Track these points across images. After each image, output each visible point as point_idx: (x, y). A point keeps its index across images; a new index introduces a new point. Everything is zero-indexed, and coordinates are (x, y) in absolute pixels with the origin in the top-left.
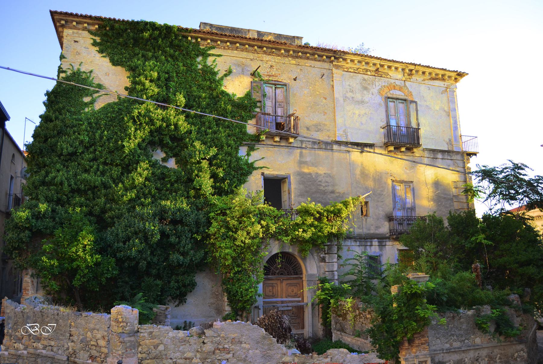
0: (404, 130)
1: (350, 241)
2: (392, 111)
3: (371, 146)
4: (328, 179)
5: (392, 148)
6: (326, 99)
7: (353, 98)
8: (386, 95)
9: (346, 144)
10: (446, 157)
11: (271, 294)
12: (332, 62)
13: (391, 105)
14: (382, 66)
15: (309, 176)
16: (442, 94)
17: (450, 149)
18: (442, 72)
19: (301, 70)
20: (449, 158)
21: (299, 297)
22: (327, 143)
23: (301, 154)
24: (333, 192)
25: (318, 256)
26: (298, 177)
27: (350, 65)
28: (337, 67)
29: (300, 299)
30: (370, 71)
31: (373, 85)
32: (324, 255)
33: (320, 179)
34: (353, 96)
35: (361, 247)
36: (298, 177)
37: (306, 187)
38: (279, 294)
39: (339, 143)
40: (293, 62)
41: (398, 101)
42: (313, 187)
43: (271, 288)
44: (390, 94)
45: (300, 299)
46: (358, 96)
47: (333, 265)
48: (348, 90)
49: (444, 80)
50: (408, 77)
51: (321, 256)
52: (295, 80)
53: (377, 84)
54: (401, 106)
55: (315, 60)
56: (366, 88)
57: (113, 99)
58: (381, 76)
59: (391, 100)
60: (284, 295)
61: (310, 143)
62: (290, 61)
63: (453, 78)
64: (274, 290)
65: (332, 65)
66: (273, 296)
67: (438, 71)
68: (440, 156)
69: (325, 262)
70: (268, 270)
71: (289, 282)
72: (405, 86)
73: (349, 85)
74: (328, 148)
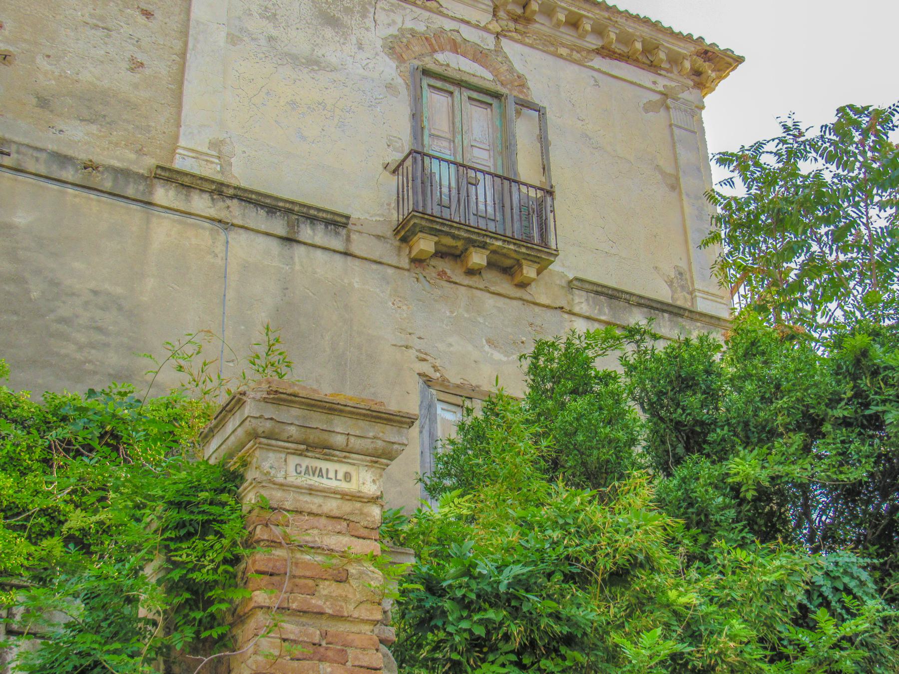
0: (484, 195)
3: (337, 222)
5: (425, 244)
6: (147, 14)
7: (270, 39)
8: (417, 63)
9: (218, 190)
15: (11, 288)
16: (647, 111)
18: (646, 32)
22: (123, 174)
31: (364, 16)
33: (64, 311)
34: (274, 33)
39: (186, 183)
41: (466, 93)
44: (436, 62)
46: (299, 40)
49: (653, 67)
50: (512, 25)
53: (382, 17)
54: (479, 121)
56: (332, 22)
57: (805, 597)
61: (43, 156)
63: (687, 65)
67: (630, 28)
72: (498, 50)
74: (130, 191)
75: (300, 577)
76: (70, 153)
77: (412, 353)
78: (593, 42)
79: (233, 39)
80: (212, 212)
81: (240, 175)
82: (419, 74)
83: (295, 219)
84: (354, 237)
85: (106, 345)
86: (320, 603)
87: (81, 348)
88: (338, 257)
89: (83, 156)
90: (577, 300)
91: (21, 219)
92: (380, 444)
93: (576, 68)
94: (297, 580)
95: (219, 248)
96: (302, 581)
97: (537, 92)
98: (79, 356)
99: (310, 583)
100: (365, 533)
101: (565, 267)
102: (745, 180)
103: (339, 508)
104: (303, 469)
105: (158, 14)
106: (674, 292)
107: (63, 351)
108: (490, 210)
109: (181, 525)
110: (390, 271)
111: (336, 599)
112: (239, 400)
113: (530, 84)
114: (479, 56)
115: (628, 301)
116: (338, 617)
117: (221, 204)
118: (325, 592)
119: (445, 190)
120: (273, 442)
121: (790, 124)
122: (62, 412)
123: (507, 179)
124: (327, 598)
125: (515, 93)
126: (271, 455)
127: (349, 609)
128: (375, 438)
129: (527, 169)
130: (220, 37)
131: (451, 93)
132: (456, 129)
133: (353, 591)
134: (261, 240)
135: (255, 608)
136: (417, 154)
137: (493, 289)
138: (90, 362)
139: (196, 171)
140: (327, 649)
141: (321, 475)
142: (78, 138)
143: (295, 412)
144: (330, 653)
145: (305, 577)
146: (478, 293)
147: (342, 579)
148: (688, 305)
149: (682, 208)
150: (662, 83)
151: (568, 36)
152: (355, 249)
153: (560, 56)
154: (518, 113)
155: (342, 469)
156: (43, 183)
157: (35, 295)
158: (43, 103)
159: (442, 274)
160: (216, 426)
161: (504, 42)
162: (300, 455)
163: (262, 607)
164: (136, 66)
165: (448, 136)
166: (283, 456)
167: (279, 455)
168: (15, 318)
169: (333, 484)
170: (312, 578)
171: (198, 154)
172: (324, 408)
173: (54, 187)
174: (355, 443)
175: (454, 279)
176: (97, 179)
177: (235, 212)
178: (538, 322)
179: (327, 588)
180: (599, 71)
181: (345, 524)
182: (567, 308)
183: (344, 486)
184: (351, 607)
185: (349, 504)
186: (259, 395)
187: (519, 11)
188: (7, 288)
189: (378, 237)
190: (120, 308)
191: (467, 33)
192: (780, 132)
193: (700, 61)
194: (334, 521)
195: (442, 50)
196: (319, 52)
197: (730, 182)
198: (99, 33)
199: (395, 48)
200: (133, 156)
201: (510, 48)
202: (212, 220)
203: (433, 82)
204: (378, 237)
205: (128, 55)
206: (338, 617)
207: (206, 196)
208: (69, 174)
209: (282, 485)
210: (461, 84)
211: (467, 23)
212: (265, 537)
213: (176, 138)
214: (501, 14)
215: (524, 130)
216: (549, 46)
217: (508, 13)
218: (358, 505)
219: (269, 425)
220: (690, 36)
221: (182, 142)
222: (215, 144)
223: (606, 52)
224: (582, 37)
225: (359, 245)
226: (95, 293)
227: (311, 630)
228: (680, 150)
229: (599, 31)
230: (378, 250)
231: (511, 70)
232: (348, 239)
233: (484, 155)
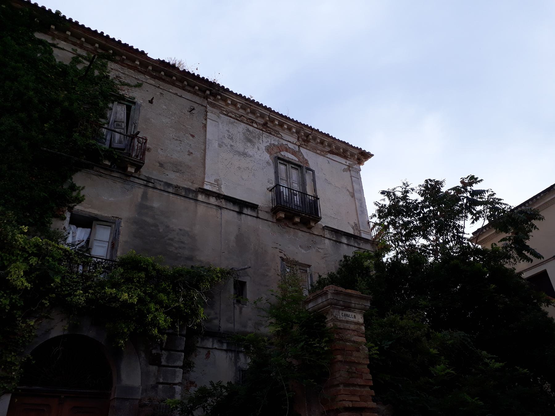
0: (297, 199)
1: (211, 340)
2: (283, 174)
3: (254, 207)
6: (193, 136)
7: (231, 146)
8: (276, 155)
9: (219, 196)
10: (352, 243)
12: (206, 98)
13: (282, 167)
14: (272, 120)
15: (153, 228)
17: (357, 234)
19: (161, 94)
20: (356, 245)
22: (188, 190)
23: (145, 196)
24: (190, 258)
27: (231, 108)
28: (213, 106)
30: (256, 123)
31: (259, 139)
32: (159, 352)
34: (232, 144)
35: (230, 354)
39: (208, 193)
40: (152, 81)
41: (291, 165)
46: (240, 147)
47: (175, 372)
48: (226, 135)
49: (345, 157)
50: (303, 143)
51: (154, 352)
52: (151, 102)
53: (264, 139)
54: (295, 174)
55: (183, 88)
56: (250, 141)
58: (270, 133)
59: (282, 162)
61: (162, 183)
62: (147, 79)
63: (356, 157)
65: (206, 101)
67: (339, 144)
68: (344, 240)
69: (159, 365)
72: (299, 151)
73: (228, 131)
74: (190, 196)
76: (171, 182)
77: (278, 250)
78: (328, 149)
79: (220, 146)
80: (216, 203)
81: (225, 191)
82: (277, 158)
83: (241, 205)
84: (259, 212)
87: (176, 248)
88: (255, 218)
89: (175, 183)
91: (156, 205)
93: (322, 157)
95: (219, 215)
97: (312, 166)
100: (361, 335)
101: (324, 222)
102: (389, 199)
105: (196, 136)
106: (354, 231)
107: (171, 250)
108: (298, 203)
110: (270, 223)
113: (309, 162)
114: (294, 153)
116: (359, 363)
117: (219, 201)
119: (285, 196)
121: (405, 182)
123: (304, 194)
125: (305, 165)
129: (309, 191)
130: (216, 145)
131: (286, 165)
132: (288, 177)
134: (232, 212)
136: (277, 185)
138: (180, 253)
139: (211, 189)
142: (173, 178)
143: (342, 297)
146: (296, 230)
147: (358, 350)
148: (359, 235)
149: (355, 203)
150: (348, 162)
151: (320, 147)
152: (260, 216)
153: (318, 153)
154: (306, 172)
155: (353, 314)
156: (162, 193)
157: (161, 230)
158: (161, 165)
159: (286, 224)
161: (301, 149)
164: (190, 154)
165: (285, 179)
169: (352, 319)
171: (211, 184)
173: (166, 194)
176: (180, 191)
177: (223, 203)
178: (314, 240)
179: (355, 354)
180: (329, 158)
187: (305, 138)
189: (266, 212)
191: (290, 145)
192: (402, 185)
193: (360, 155)
195: (283, 151)
196: (246, 151)
197: (384, 200)
198: (178, 142)
199: (269, 149)
200: (190, 184)
201: (303, 150)
202: (216, 206)
203: (281, 161)
204: (266, 212)
205: (187, 150)
207: (214, 198)
208: (170, 190)
210: (289, 162)
211: (290, 142)
213: (204, 178)
214: (300, 139)
215: (308, 178)
216: (314, 150)
217: (302, 139)
219: (335, 301)
220: (357, 147)
221: (206, 180)
222: (216, 181)
223: (331, 152)
224: (324, 147)
225: (261, 215)
226: (180, 230)
228: (354, 184)
229: (330, 145)
230: (266, 216)
231: (303, 158)
232: (258, 213)
233: (296, 185)
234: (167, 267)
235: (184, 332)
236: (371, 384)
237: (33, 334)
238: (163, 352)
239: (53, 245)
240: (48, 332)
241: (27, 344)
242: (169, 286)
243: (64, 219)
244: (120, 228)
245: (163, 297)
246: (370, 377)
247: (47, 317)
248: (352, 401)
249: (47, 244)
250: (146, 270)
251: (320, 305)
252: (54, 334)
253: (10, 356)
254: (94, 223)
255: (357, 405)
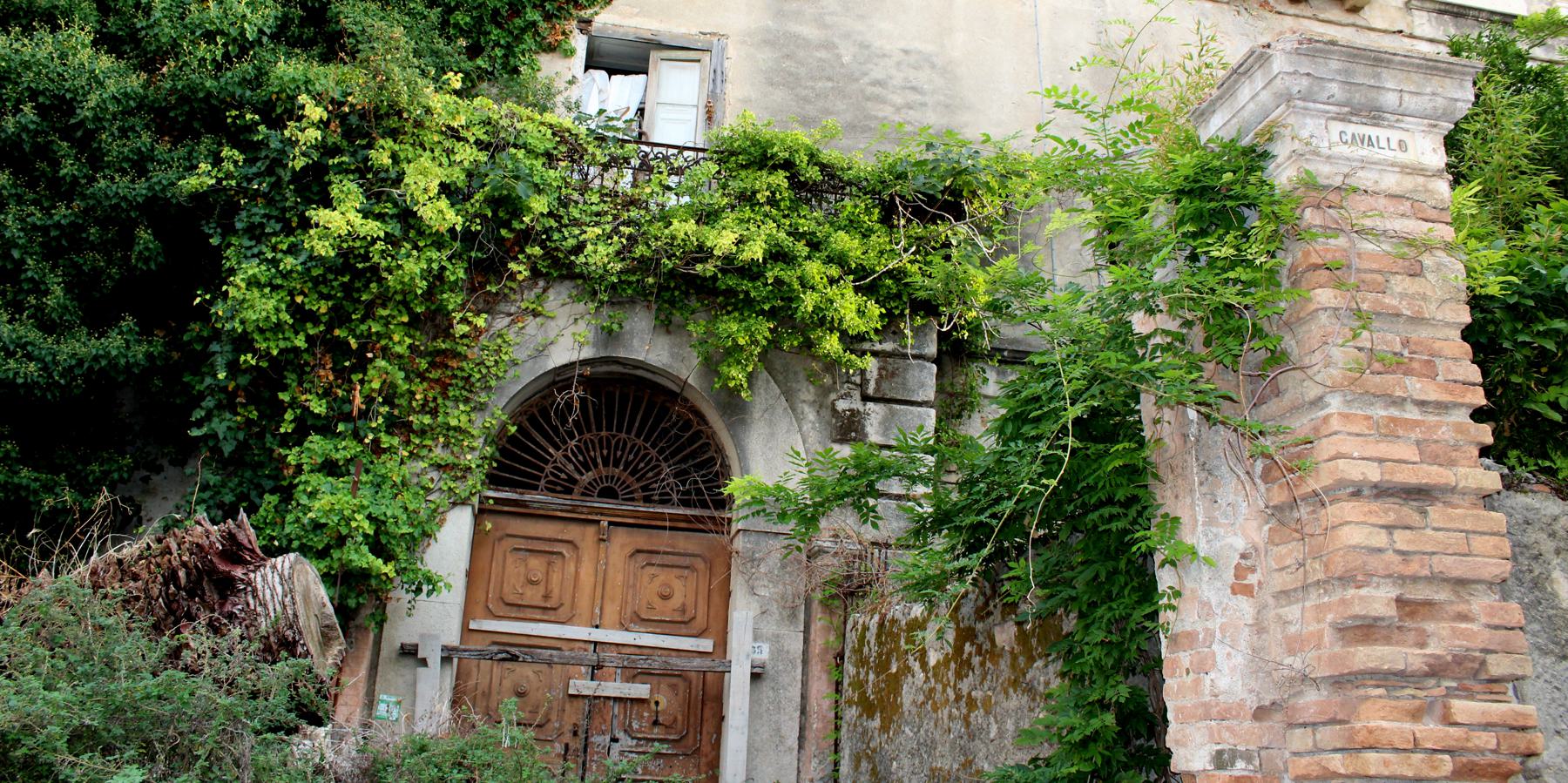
4: (923, 77)
11: (533, 596)
15: (823, 54)
21: (699, 635)
25: (819, 405)
26: (765, 56)
29: (706, 645)
32: (857, 404)
33: (878, 74)
36: (765, 56)
37: (806, 100)
38: (584, 601)
42: (841, 106)
43: (536, 563)
45: (706, 645)
51: (842, 405)
60: (611, 611)
64: (555, 578)
66: (547, 611)
70: (516, 463)
71: (642, 539)
75: (1365, 271)
85: (924, 105)
86: (1395, 302)
87: (898, 110)
90: (1417, 21)
92: (1440, 101)
94: (1363, 276)
96: (1368, 277)
98: (897, 118)
99: (1379, 278)
100: (1433, 214)
103: (1398, 184)
104: (1349, 137)
107: (881, 114)
109: (1198, 217)
111: (1412, 297)
112: (1262, 54)
115: (1476, 18)
116: (1417, 320)
118: (1399, 289)
120: (1311, 105)
122: (900, 169)
124: (1403, 296)
126: (1308, 121)
127: (1430, 310)
128: (1434, 94)
133: (1431, 285)
135: (1317, 310)
137: (1322, 16)
140: (1411, 359)
141: (1370, 143)
144: (1415, 365)
145: (1372, 271)
155: (1396, 136)
157: (846, 59)
160: (1220, 98)
162: (1342, 120)
163: (1326, 309)
166: (1323, 121)
167: (1317, 121)
168: (830, 84)
169: (1388, 155)
170: (1379, 272)
172: (1368, 58)
174: (1411, 103)
175: (1279, 8)
181: (1408, 204)
182: (1407, 31)
183: (1401, 157)
184: (1433, 307)
185: (1409, 178)
186: (1288, 47)
188: (818, 55)
190: (933, 66)
194: (1394, 201)
206: (1417, 320)
209: (1329, 157)
212: (1318, 222)
218: (1421, 180)
226: (906, 52)
227: (1390, 337)
234: (860, 157)
235: (932, 349)
236: (1479, 398)
237: (505, 358)
238: (870, 405)
239: (529, 118)
240: (541, 351)
241: (493, 383)
242: (868, 211)
243: (568, 53)
244: (726, 64)
245: (844, 241)
246: (1475, 373)
247: (535, 314)
248: (1381, 461)
249: (512, 115)
250: (788, 165)
251: (1245, 114)
252: (561, 355)
253: (456, 413)
254: (654, 55)
255: (1406, 476)
